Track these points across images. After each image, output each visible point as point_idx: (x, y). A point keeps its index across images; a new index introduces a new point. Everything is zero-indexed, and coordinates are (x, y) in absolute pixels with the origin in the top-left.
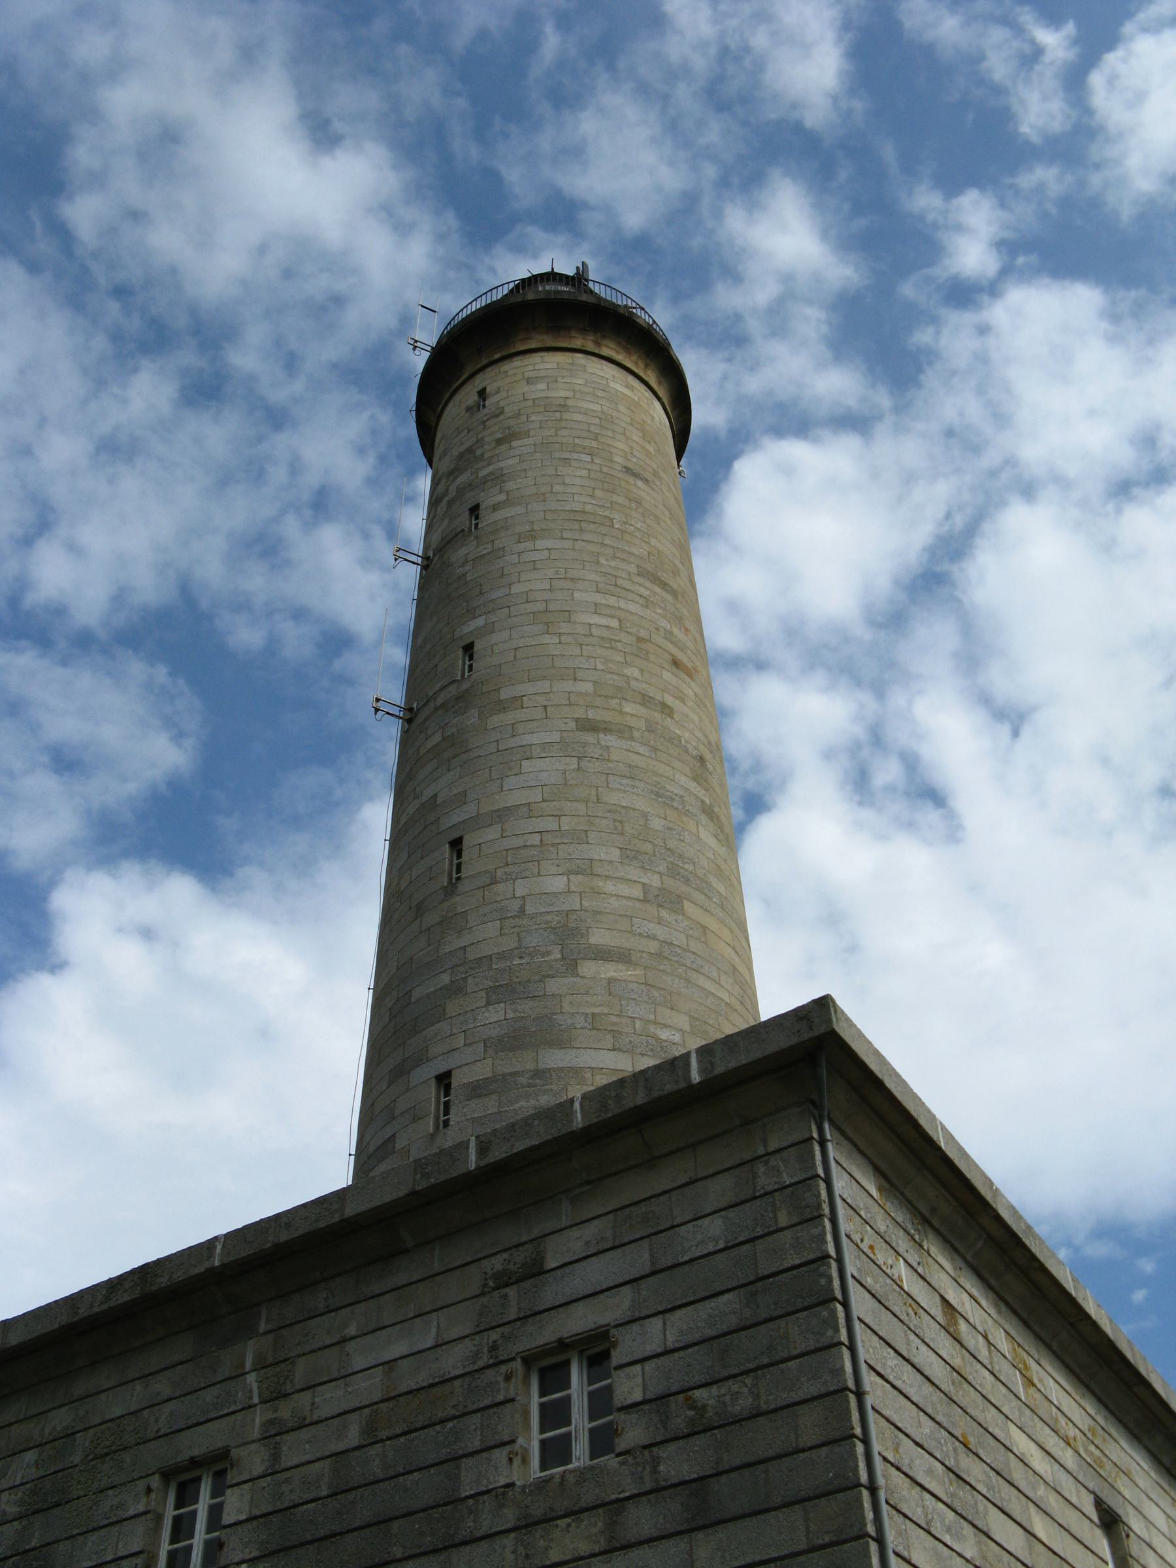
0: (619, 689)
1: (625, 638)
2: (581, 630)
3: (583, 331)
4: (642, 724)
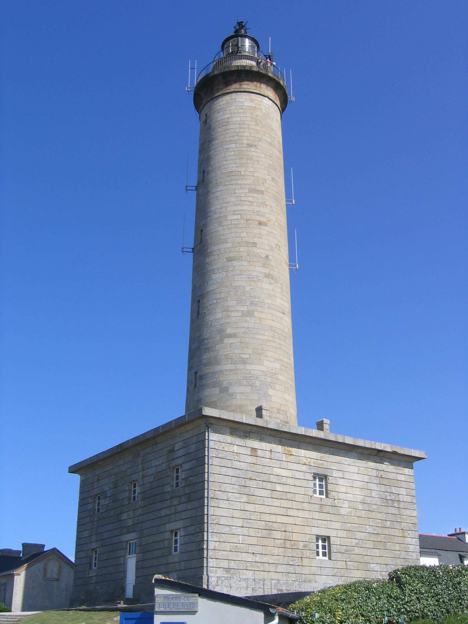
0: (239, 243)
1: (242, 222)
2: (229, 223)
3: (235, 82)
4: (246, 254)
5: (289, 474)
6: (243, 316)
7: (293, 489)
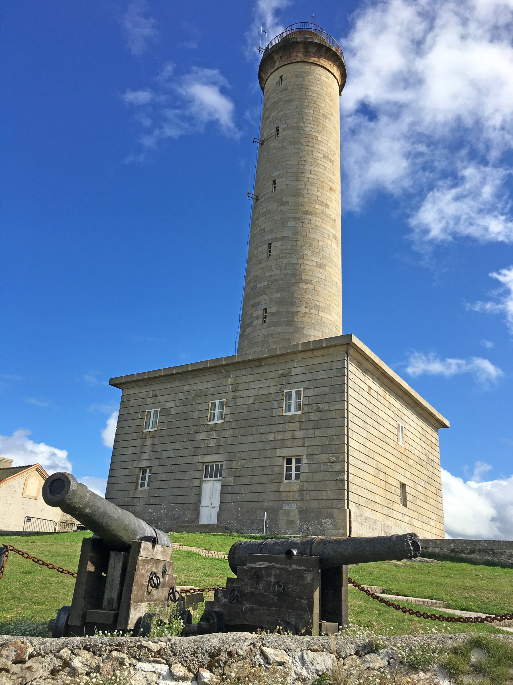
3: (315, 55)
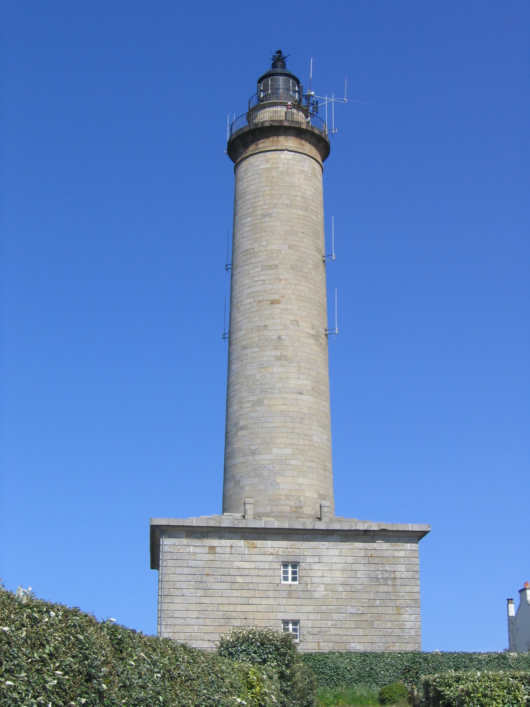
0: (251, 329)
3: (252, 142)
4: (256, 340)
5: (253, 565)
6: (253, 406)
7: (256, 579)
